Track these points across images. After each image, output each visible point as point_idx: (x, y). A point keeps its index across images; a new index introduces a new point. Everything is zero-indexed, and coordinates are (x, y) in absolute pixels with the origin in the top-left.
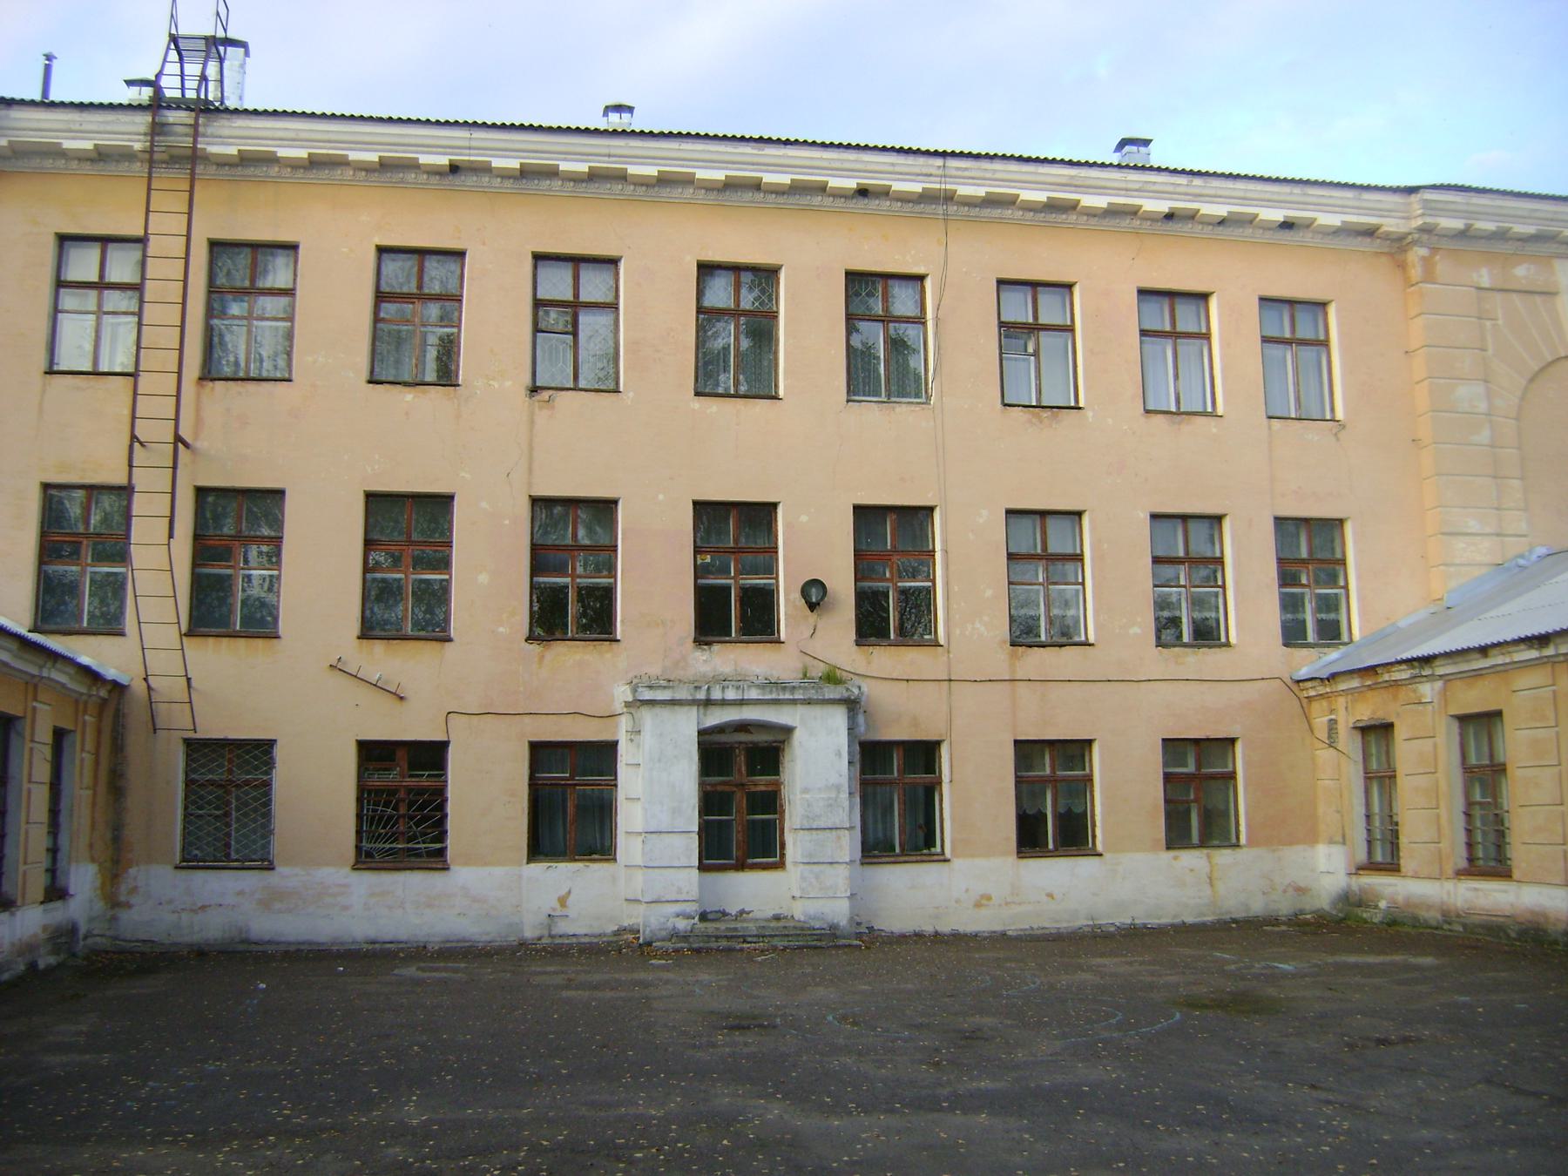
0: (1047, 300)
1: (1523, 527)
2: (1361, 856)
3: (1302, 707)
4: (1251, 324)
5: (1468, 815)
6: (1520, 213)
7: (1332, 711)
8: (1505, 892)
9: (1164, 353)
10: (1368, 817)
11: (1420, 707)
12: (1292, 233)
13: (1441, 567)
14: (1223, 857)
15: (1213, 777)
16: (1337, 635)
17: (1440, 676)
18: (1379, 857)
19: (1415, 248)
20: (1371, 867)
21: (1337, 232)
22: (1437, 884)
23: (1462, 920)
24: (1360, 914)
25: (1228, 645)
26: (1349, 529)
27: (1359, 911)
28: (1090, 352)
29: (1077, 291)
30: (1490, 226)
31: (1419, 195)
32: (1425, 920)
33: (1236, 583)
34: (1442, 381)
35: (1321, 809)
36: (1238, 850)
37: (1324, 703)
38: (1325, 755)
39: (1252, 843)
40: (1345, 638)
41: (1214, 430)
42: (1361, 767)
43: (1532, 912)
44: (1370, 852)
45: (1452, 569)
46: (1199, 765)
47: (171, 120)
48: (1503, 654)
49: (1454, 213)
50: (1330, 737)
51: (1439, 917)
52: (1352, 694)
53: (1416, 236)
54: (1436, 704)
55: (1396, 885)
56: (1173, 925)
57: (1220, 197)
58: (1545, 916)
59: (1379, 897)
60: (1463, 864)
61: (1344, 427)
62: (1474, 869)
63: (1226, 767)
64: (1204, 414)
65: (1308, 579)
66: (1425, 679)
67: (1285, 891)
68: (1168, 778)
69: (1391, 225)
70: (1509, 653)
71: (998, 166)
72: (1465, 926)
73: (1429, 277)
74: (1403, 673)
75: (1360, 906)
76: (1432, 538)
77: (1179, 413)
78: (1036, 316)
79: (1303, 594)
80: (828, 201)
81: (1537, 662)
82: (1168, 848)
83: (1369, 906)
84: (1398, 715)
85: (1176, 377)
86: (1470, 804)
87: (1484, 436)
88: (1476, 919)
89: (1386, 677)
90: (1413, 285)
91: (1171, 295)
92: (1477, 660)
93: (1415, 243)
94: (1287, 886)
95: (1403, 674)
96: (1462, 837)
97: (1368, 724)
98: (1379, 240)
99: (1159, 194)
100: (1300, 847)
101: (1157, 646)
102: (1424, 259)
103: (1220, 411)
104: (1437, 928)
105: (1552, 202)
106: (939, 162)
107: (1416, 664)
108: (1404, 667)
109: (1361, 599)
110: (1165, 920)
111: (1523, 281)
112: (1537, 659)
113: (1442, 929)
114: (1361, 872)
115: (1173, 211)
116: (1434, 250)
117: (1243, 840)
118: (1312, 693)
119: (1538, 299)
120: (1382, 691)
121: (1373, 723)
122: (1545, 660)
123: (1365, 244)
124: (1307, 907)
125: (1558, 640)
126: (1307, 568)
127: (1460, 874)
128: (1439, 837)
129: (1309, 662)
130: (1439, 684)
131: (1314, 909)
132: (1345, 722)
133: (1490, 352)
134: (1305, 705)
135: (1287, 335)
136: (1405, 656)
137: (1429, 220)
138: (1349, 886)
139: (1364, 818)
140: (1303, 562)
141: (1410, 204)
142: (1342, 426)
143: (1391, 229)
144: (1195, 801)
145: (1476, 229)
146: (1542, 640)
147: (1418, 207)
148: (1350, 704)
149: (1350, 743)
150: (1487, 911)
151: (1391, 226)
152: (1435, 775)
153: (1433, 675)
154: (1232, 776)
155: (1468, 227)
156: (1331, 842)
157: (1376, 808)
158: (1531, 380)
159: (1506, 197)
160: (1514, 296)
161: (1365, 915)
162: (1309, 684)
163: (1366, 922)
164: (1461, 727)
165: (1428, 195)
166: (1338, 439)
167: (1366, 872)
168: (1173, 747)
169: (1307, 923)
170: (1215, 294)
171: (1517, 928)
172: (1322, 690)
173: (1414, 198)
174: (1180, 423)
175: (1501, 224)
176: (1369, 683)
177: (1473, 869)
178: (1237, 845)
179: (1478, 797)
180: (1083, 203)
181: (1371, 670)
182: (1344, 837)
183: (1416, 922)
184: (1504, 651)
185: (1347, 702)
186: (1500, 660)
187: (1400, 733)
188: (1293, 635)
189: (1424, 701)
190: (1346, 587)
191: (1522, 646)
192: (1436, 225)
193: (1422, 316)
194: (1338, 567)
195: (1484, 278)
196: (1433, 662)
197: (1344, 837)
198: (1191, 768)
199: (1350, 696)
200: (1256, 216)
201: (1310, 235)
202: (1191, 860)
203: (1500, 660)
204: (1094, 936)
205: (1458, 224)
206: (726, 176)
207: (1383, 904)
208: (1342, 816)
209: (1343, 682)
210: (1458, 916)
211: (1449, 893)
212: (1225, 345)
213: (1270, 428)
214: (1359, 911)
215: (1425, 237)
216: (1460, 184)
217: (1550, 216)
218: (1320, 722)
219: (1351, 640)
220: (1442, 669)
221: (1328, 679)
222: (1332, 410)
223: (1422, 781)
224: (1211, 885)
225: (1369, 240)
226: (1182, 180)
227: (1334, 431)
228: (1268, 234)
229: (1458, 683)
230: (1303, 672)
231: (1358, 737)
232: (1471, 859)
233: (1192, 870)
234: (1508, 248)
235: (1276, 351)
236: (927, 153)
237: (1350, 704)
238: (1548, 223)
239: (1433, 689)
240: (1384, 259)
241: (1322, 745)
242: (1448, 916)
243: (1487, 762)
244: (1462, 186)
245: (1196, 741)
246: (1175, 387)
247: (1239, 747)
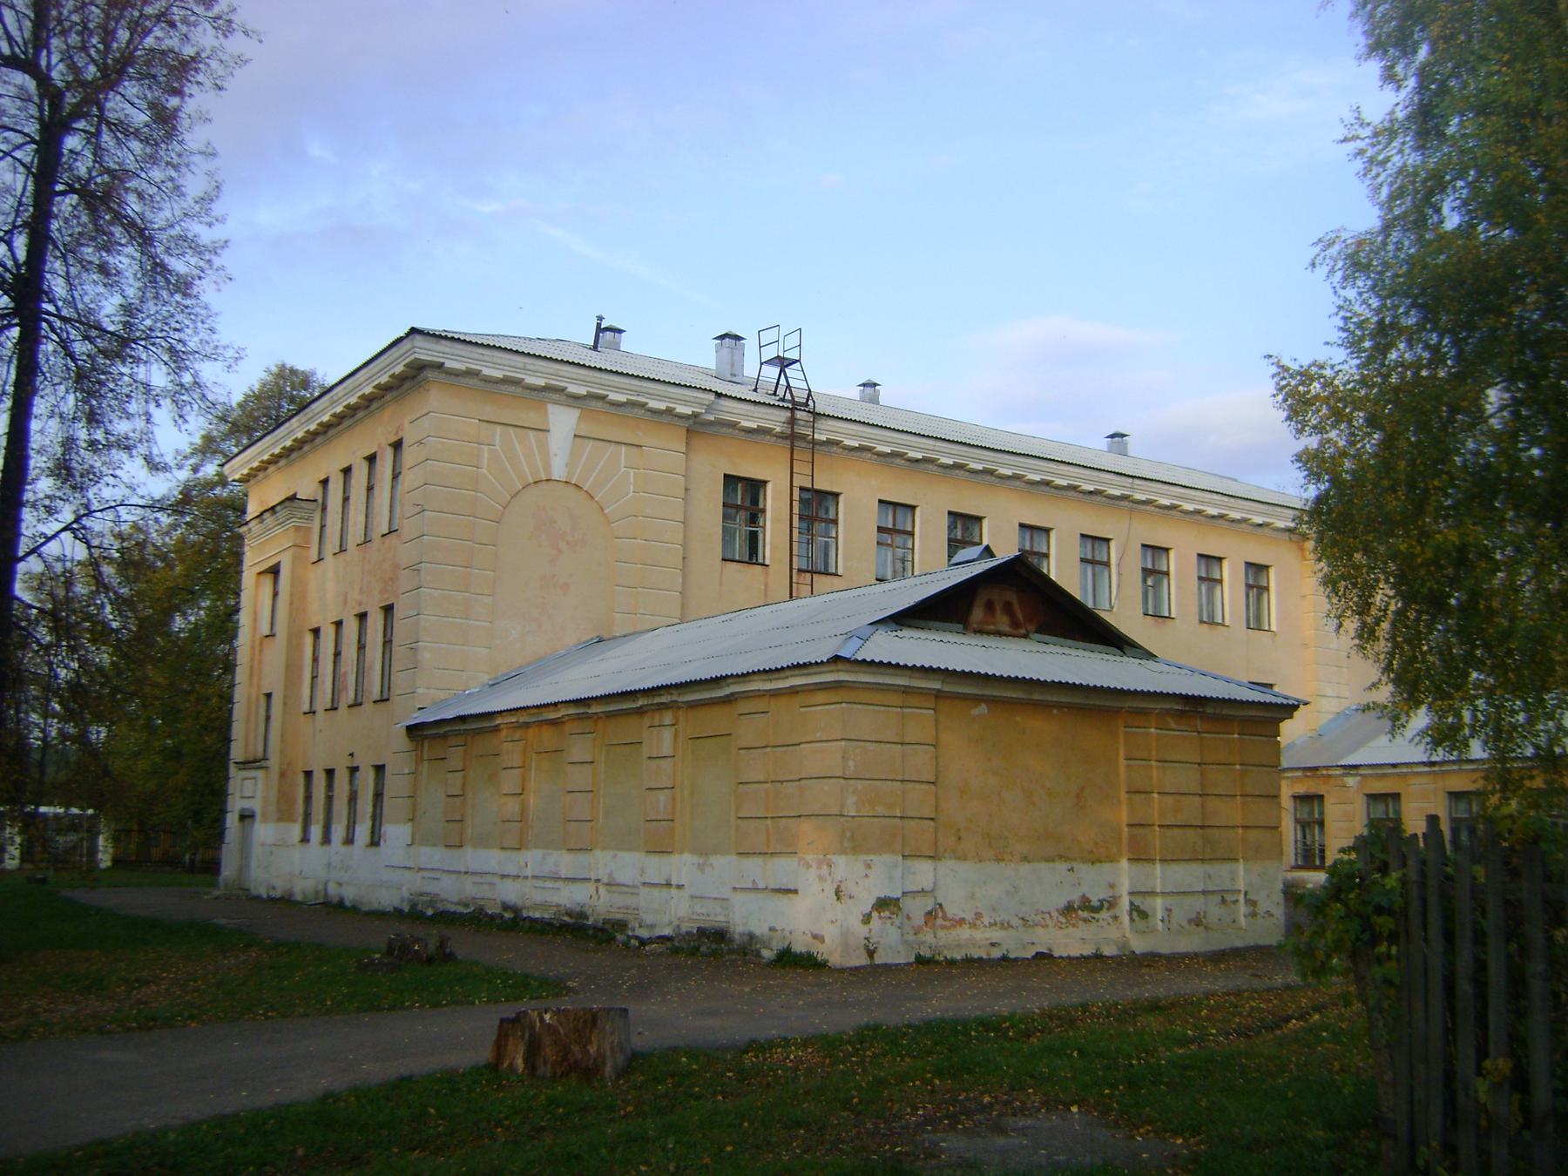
2: (1292, 862)
27: (1294, 890)
28: (1178, 588)
29: (1053, 535)
42: (1293, 817)
44: (1296, 860)
47: (798, 417)
71: (496, 353)
78: (1032, 547)
80: (1076, 494)
84: (1328, 792)
89: (1324, 772)
91: (895, 505)
95: (1339, 772)
99: (1215, 505)
106: (1130, 480)
130: (1358, 778)
152: (522, 797)
160: (511, 430)
175: (468, 365)
180: (526, 381)
181: (1316, 768)
186: (1405, 770)
203: (1405, 770)
220: (1362, 772)
226: (1226, 499)
236: (1128, 476)
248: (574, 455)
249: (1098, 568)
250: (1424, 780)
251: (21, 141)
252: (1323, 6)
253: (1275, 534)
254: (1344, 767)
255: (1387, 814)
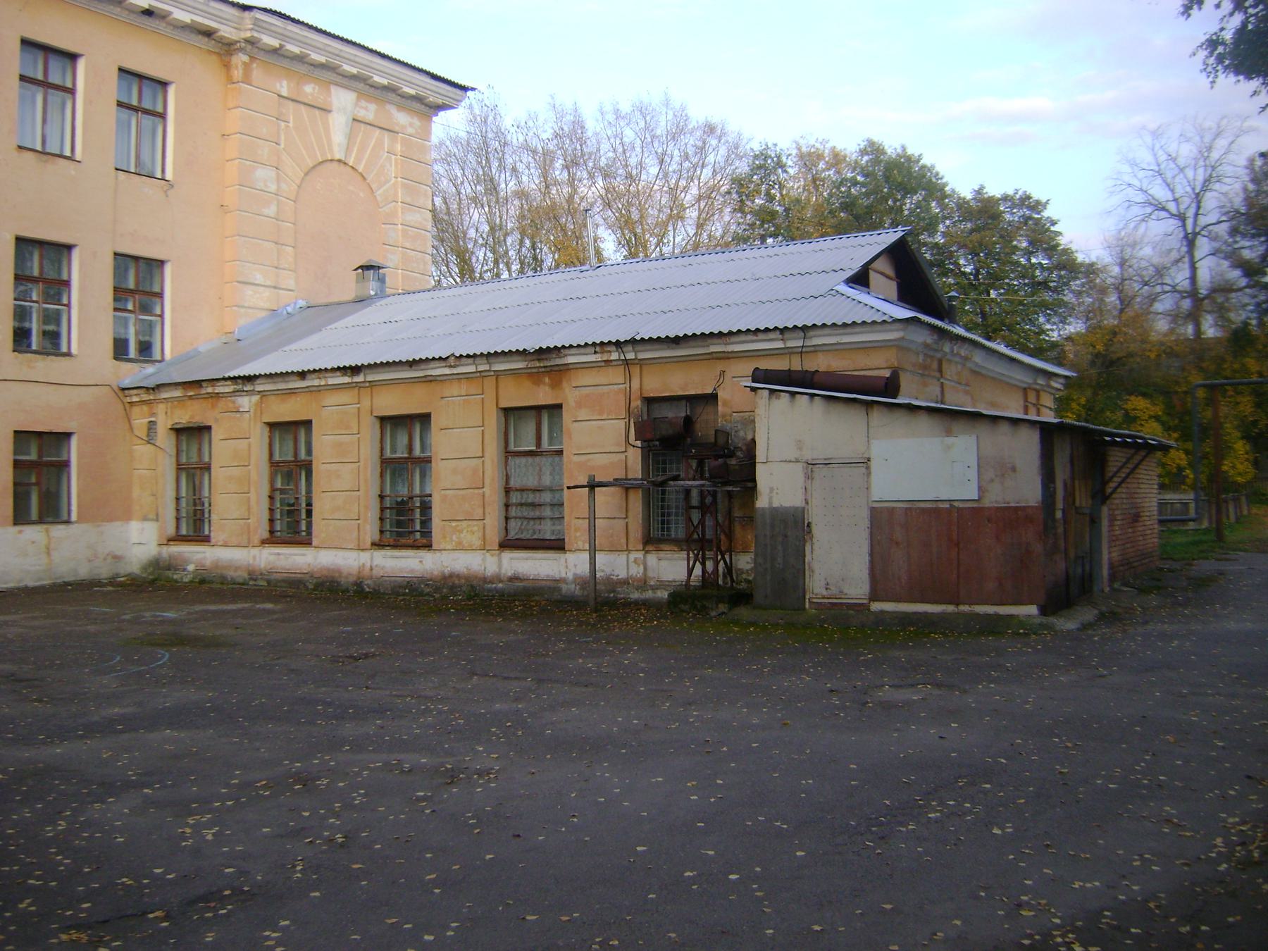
0: (55, 64)
1: (291, 283)
2: (171, 530)
3: (125, 410)
4: (111, 88)
5: (271, 498)
6: (319, 45)
7: (153, 414)
8: (304, 555)
9: (34, 102)
10: (178, 499)
11: (238, 415)
12: (150, 19)
13: (234, 308)
14: (58, 531)
15: (52, 464)
16: (57, 345)
17: (259, 391)
18: (184, 532)
19: (240, 54)
20: (178, 538)
21: (186, 27)
22: (245, 550)
23: (266, 577)
24: (171, 575)
25: (68, 354)
26: (168, 269)
27: (169, 573)
30: (296, 50)
31: (252, 14)
32: (232, 578)
33: (81, 304)
34: (248, 163)
35: (136, 492)
36: (71, 526)
37: (145, 408)
38: (143, 450)
39: (81, 519)
40: (157, 356)
41: (73, 173)
42: (174, 460)
43: (328, 570)
44: (178, 527)
45: (243, 310)
46: (40, 455)
48: (320, 378)
49: (274, 34)
50: (148, 435)
51: (246, 576)
52: (172, 402)
53: (243, 45)
54: (252, 413)
55: (204, 553)
56: (18, 589)
57: (413, 84)
58: (339, 571)
59: (187, 562)
60: (266, 535)
61: (172, 186)
62: (273, 539)
63: (29, 454)
64: (61, 156)
65: (134, 306)
66: (245, 393)
67: (105, 559)
68: (17, 464)
69: (226, 32)
70: (326, 377)
72: (269, 582)
73: (247, 79)
74: (226, 387)
75: (169, 570)
76: (228, 285)
77: (44, 153)
79: (31, 307)
81: (347, 386)
82: (15, 524)
83: (176, 570)
84: (217, 420)
85: (44, 121)
86: (273, 489)
87: (271, 210)
88: (278, 576)
89: (210, 390)
90: (234, 83)
91: (141, 77)
92: (295, 381)
93: (241, 50)
94: (108, 555)
95: (227, 388)
96: (266, 516)
97: (186, 426)
98: (213, 42)
100: (118, 523)
101: (14, 351)
102: (244, 63)
103: (78, 156)
104: (243, 584)
105: (341, 42)
107: (239, 381)
108: (229, 383)
109: (173, 326)
110: (11, 585)
111: (310, 97)
112: (348, 383)
113: (248, 584)
114: (172, 543)
115: (151, 9)
116: (252, 58)
117: (74, 517)
118: (135, 399)
119: (317, 112)
120: (201, 400)
121: (191, 425)
122: (354, 385)
123: (202, 42)
124: (122, 572)
125: (368, 371)
126: (134, 297)
127: (264, 542)
128: (249, 515)
129: (131, 374)
130: (256, 398)
131: (127, 573)
132: (164, 422)
133: (282, 146)
134: (128, 409)
135: (135, 102)
136: (232, 374)
137: (256, 34)
138: (160, 554)
139: (175, 501)
140: (132, 291)
141: (243, 18)
142: (171, 185)
143: (226, 35)
144: (37, 484)
145: (287, 50)
146: (355, 370)
147: (249, 22)
148: (169, 411)
149: (165, 439)
150: (289, 570)
151: (226, 32)
153: (253, 390)
154: (66, 464)
155: (281, 46)
156: (145, 519)
157: (183, 493)
158: (306, 174)
159: (312, 31)
160: (302, 107)
161: (175, 577)
162: (135, 392)
163: (176, 581)
164: (270, 431)
165: (259, 15)
166: (167, 196)
167: (175, 543)
168: (21, 437)
169: (121, 584)
170: (84, 57)
171: (315, 581)
172: (145, 397)
173: (247, 14)
174: (46, 162)
175: (304, 50)
176: (191, 393)
177: (274, 539)
178: (68, 522)
179: (279, 485)
180: (221, 33)
181: (198, 383)
182: (157, 515)
183: (223, 580)
184: (321, 376)
185: (167, 408)
187: (217, 434)
188: (120, 348)
189: (241, 410)
190: (162, 316)
191: (338, 374)
192: (260, 40)
193: (240, 109)
194: (154, 299)
195: (284, 88)
196: (255, 381)
197: (157, 515)
198: (33, 456)
199: (170, 404)
200: (170, 13)
201: (164, 25)
202: (33, 533)
203: (316, 382)
204: (871, 528)
205: (275, 43)
206: (192, 20)
207: (191, 568)
208: (157, 499)
209: (166, 392)
210: (261, 574)
211: (254, 558)
212: (88, 102)
213: (116, 178)
214: (169, 573)
215: (249, 47)
216: (283, 12)
217: (337, 52)
218: (140, 422)
219: (162, 360)
220: (260, 386)
221: (153, 389)
222: (163, 171)
223: (236, 472)
224: (48, 554)
225: (206, 39)
227: (165, 188)
228: (132, 16)
229: (273, 398)
230: (127, 383)
231: (173, 436)
232: (272, 532)
233: (33, 542)
234: (303, 69)
235: (125, 113)
237: (169, 411)
238: (334, 57)
239: (250, 402)
240: (214, 57)
241: (140, 441)
242: (253, 575)
243: (291, 458)
244: (284, 15)
245: (40, 434)
246: (136, 152)
247: (74, 441)
248: (351, 137)
249: (55, 96)
250: (344, 397)
251: (1187, 266)
252: (1187, 11)
253: (169, 31)
254: (234, 379)
255: (296, 454)
